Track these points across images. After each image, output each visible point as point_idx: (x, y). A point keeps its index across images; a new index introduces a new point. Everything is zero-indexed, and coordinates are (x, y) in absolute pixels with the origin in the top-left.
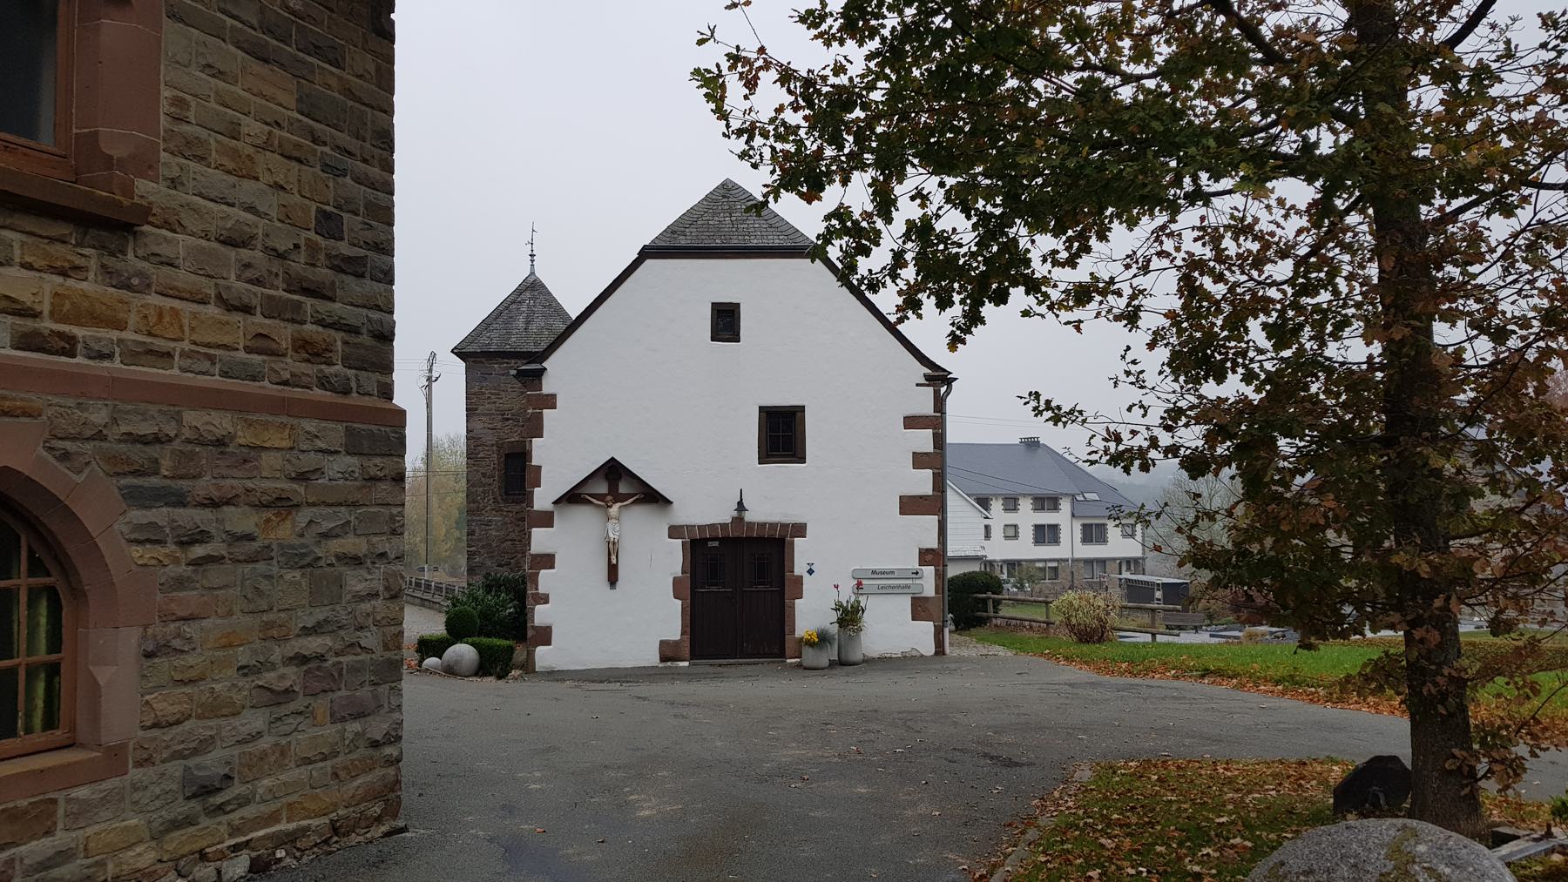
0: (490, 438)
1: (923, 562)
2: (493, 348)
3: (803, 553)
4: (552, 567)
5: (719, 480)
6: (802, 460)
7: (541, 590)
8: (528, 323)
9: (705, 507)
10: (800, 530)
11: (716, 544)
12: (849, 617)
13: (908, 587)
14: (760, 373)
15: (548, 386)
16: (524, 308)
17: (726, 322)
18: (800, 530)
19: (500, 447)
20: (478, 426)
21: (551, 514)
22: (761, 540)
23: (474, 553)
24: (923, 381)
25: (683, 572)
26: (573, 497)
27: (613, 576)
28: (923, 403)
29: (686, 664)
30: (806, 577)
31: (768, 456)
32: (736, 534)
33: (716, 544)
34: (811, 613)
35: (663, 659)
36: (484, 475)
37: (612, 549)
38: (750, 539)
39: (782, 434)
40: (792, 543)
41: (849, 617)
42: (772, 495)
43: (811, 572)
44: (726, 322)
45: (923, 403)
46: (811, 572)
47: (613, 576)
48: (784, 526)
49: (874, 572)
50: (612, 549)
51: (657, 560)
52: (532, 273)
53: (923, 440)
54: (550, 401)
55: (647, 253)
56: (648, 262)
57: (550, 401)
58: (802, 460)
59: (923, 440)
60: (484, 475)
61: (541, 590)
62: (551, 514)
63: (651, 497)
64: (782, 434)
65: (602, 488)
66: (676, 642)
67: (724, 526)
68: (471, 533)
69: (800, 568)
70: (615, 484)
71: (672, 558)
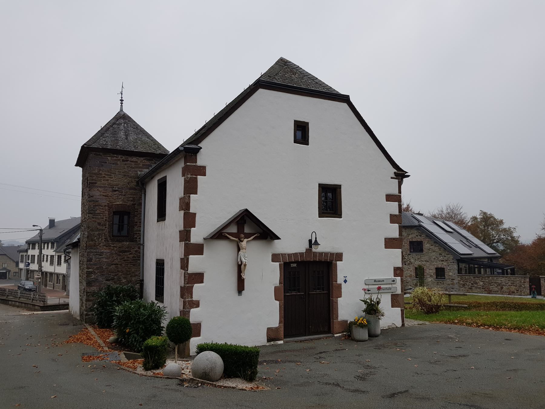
0: (104, 202)
1: (396, 275)
2: (109, 147)
3: (342, 270)
4: (202, 282)
5: (297, 228)
6: (340, 216)
7: (195, 298)
8: (127, 136)
9: (291, 244)
10: (339, 257)
11: (295, 265)
12: (372, 309)
13: (390, 289)
14: (323, 162)
15: (200, 162)
16: (122, 127)
17: (302, 133)
18: (339, 257)
19: (110, 207)
20: (96, 193)
21: (203, 245)
22: (320, 262)
23: (91, 273)
24: (394, 176)
25: (280, 283)
26: (219, 235)
27: (241, 286)
28: (392, 187)
29: (282, 342)
30: (343, 284)
31: (323, 213)
32: (308, 259)
33: (295, 265)
34: (348, 306)
35: (269, 341)
36: (99, 224)
37: (240, 268)
38: (315, 262)
39: (330, 201)
40: (336, 265)
41: (372, 309)
42: (330, 235)
43: (345, 281)
44: (302, 133)
45: (392, 187)
46: (345, 281)
47: (241, 286)
48: (332, 254)
49: (375, 281)
50: (240, 268)
51: (265, 275)
52: (121, 110)
53: (393, 207)
54: (202, 171)
55: (262, 84)
56: (261, 91)
57: (202, 171)
58: (340, 216)
59: (393, 207)
60: (99, 224)
61: (195, 298)
62: (203, 245)
63: (266, 235)
64: (330, 201)
65: (234, 229)
66: (276, 328)
67: (301, 254)
68: (90, 260)
69: (340, 280)
70: (247, 227)
71: (273, 274)
